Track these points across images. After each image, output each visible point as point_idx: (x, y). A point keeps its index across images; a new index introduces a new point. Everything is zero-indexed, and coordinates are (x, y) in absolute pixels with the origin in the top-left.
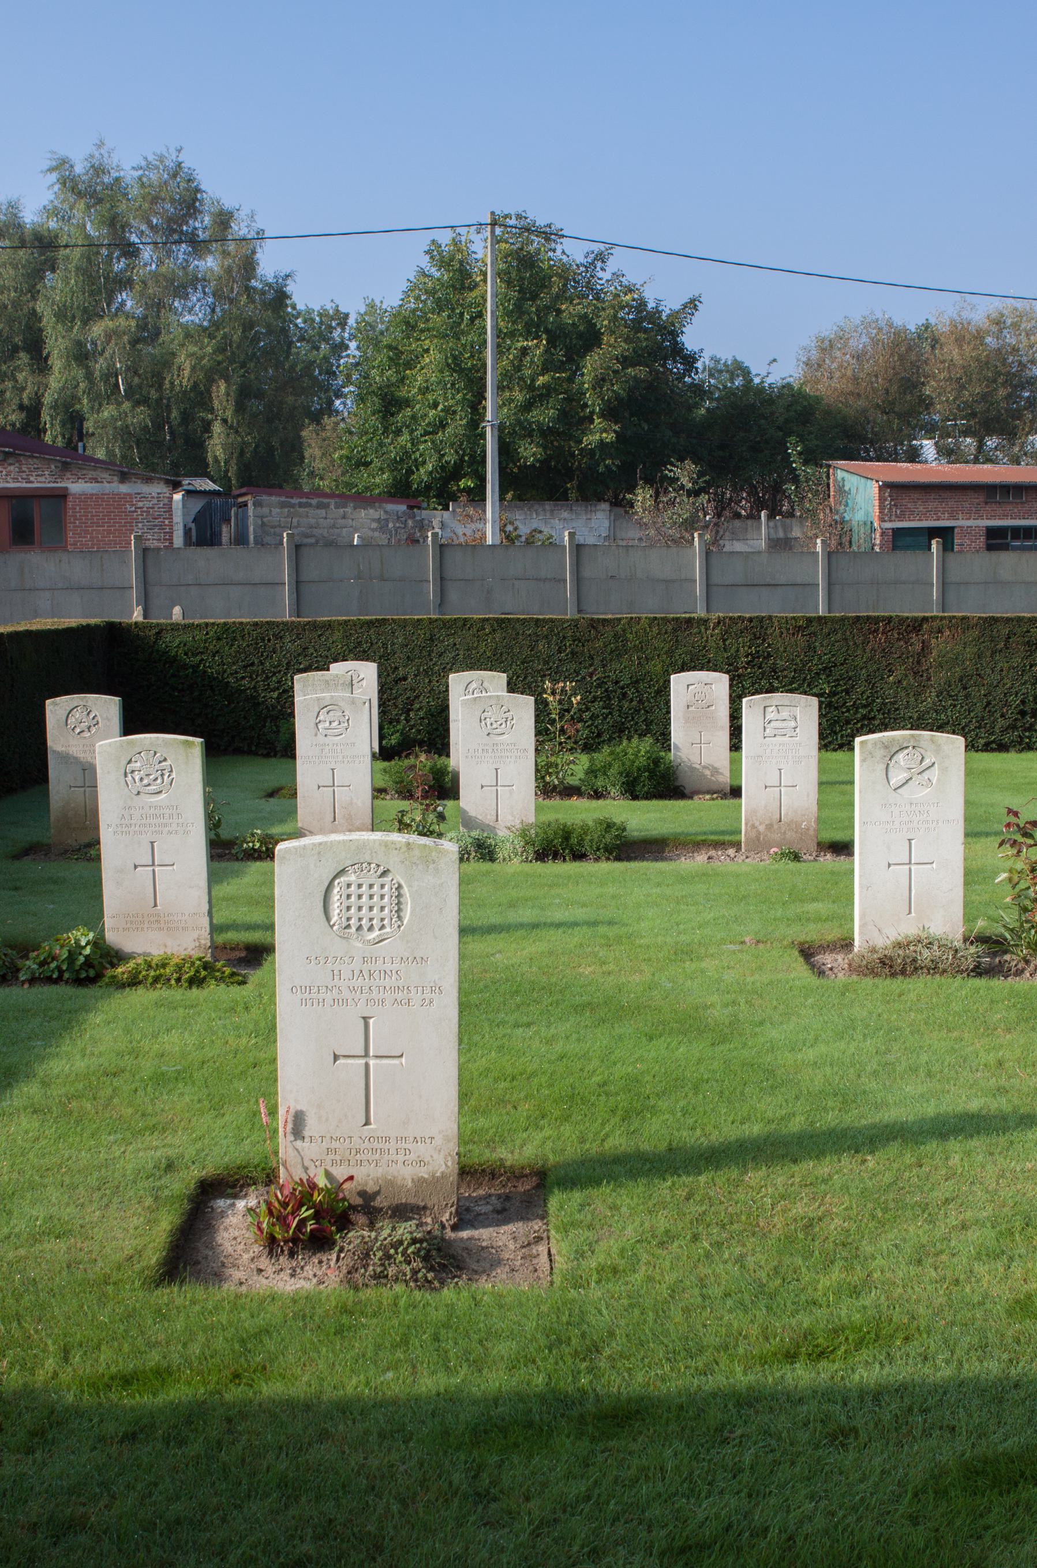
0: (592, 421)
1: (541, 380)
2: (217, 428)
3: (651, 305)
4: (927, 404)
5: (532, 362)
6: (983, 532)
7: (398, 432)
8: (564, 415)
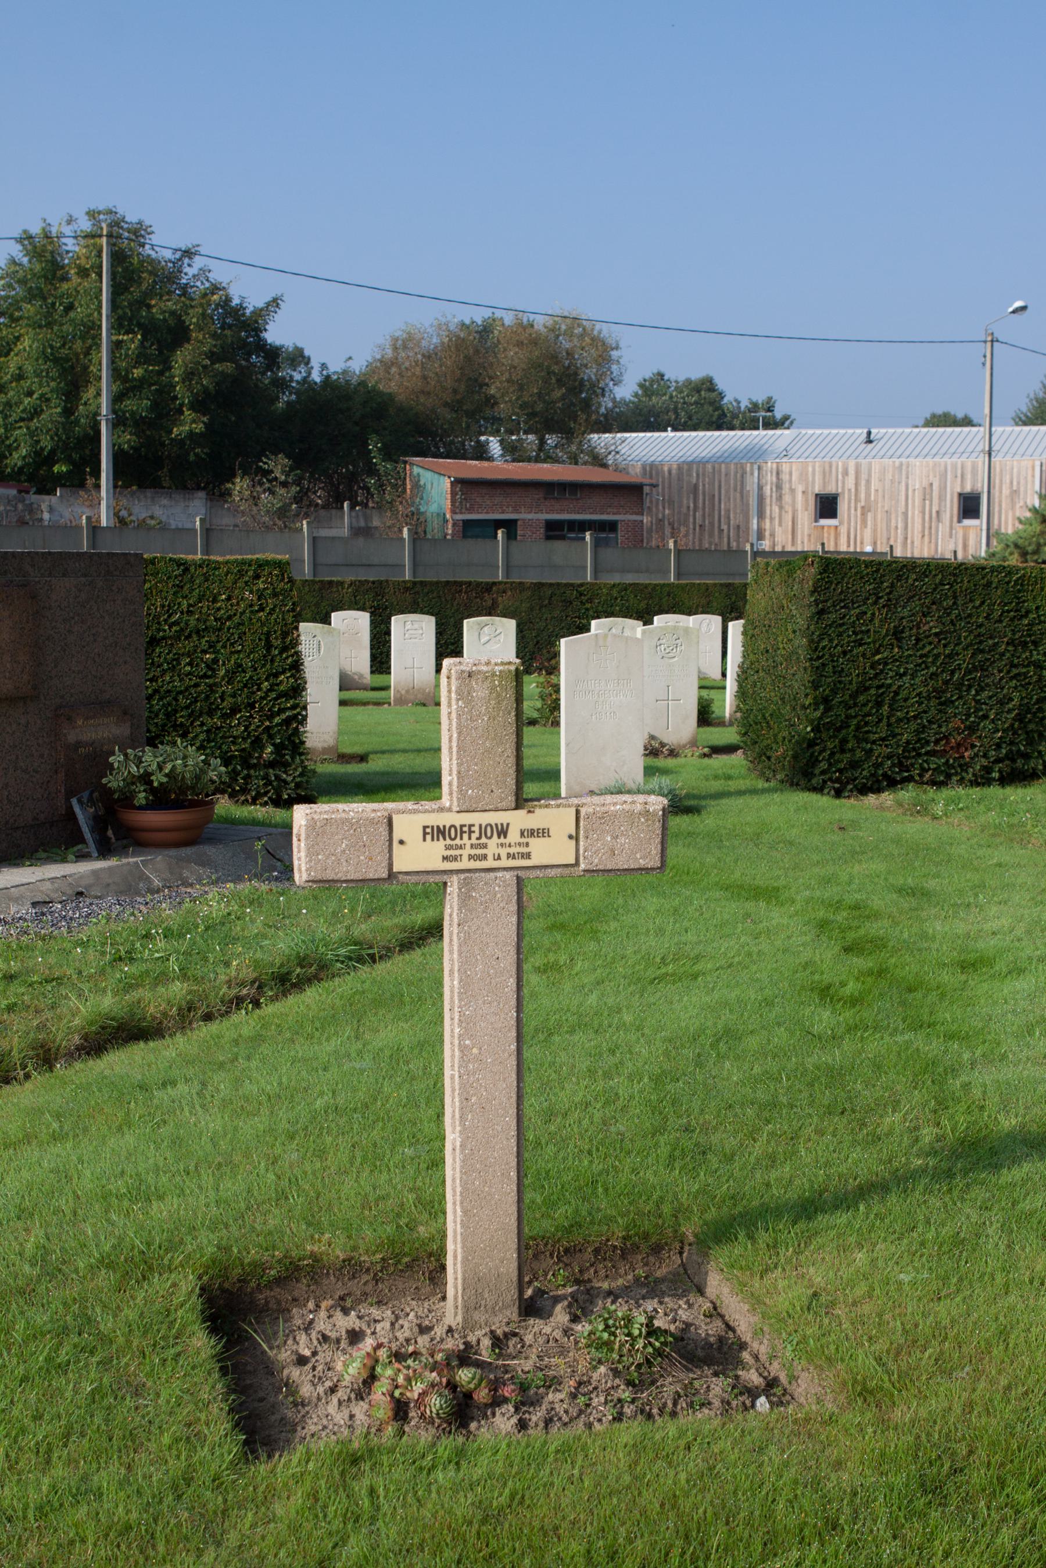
0: (182, 413)
1: (137, 372)
3: (236, 301)
4: (491, 402)
5: (127, 355)
6: (543, 525)
8: (155, 406)
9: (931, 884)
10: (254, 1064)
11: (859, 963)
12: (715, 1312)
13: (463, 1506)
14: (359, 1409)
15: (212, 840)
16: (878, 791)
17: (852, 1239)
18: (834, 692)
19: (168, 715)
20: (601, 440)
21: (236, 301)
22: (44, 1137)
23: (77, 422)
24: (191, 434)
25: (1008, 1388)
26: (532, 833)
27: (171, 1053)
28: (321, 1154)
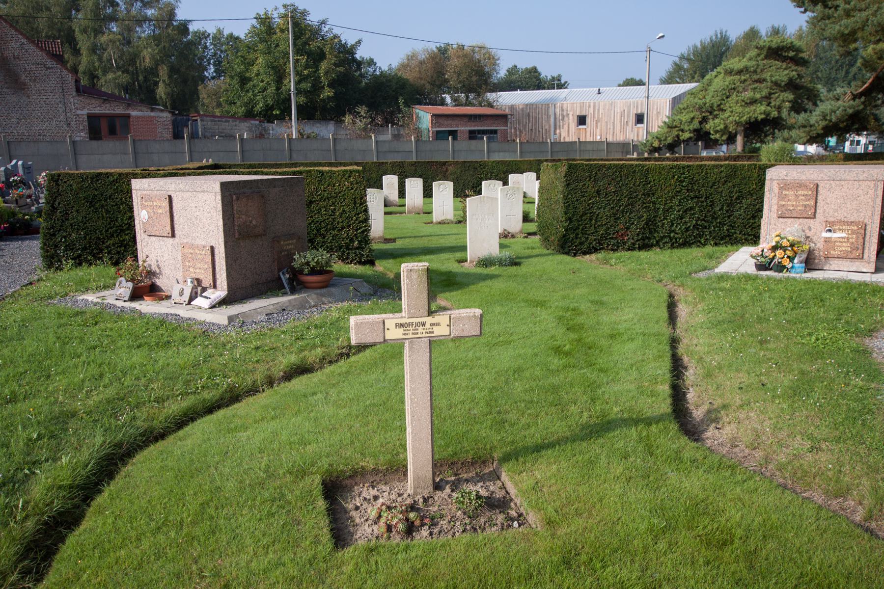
1: (306, 72)
2: (161, 85)
3: (343, 42)
4: (446, 81)
7: (248, 91)
8: (313, 85)
9: (605, 298)
10: (346, 384)
11: (573, 336)
12: (503, 487)
13: (407, 569)
14: (375, 528)
15: (334, 285)
16: (591, 253)
17: (552, 460)
18: (573, 215)
19: (317, 230)
20: (491, 96)
21: (343, 42)
22: (268, 418)
23: (282, 93)
24: (328, 97)
25: (599, 522)
26: (434, 324)
27: (316, 380)
28: (367, 424)
